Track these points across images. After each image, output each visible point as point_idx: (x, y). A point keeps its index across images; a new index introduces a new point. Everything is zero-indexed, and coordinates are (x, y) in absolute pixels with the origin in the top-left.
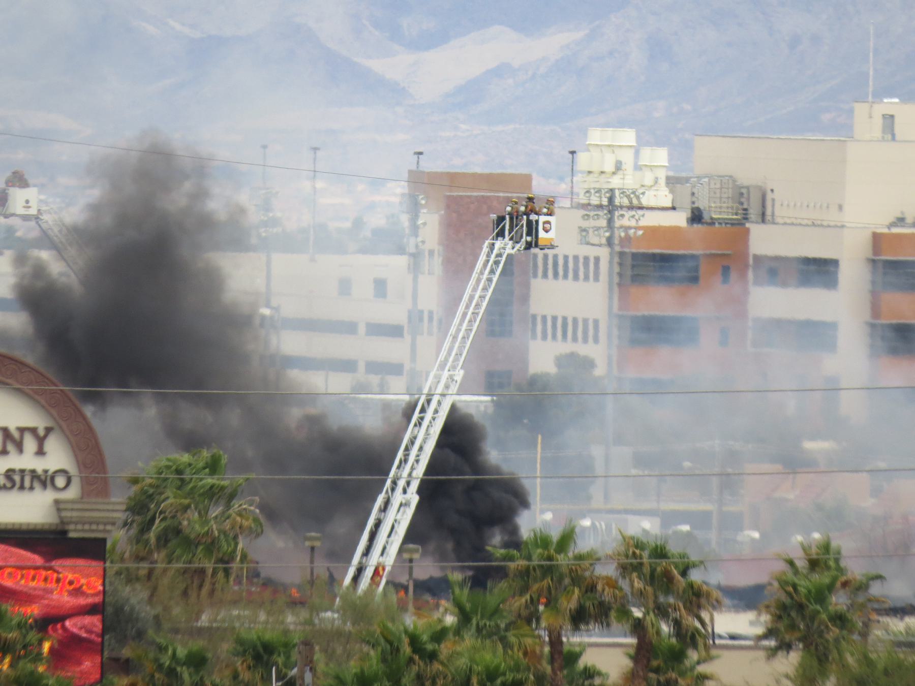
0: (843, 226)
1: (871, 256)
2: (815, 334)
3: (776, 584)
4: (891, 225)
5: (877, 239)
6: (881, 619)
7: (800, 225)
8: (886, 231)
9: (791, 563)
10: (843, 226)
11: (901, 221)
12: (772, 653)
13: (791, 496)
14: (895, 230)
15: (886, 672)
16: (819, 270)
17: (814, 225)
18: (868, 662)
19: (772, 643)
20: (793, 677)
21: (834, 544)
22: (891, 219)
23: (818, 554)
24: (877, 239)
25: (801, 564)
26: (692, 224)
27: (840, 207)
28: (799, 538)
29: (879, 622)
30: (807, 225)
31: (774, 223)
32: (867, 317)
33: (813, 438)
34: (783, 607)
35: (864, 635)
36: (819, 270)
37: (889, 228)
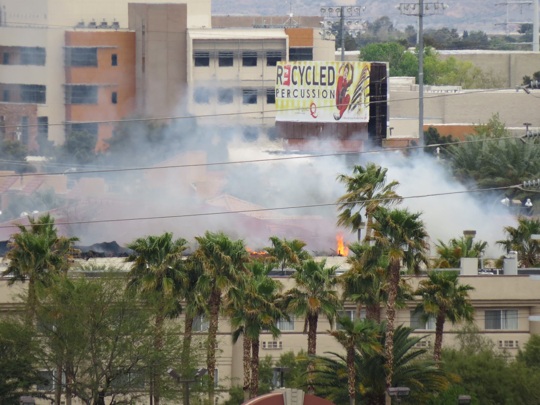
0: (47, 28)
1: (64, 46)
2: (37, 94)
3: (13, 241)
4: (77, 27)
5: (68, 36)
6: (77, 260)
7: (21, 27)
8: (72, 30)
9: (23, 229)
10: (47, 28)
11: (81, 24)
12: (12, 281)
13: (21, 189)
14: (78, 30)
15: (78, 291)
16: (38, 56)
17: (30, 27)
18: (69, 284)
19: (11, 276)
20: (345, 358)
21: (51, 218)
22: (75, 24)
23: (39, 223)
24: (68, 36)
25: (29, 228)
26: (524, 78)
27: (45, 17)
28: (26, 214)
29: (73, 261)
30: (26, 27)
31: (6, 26)
32: (64, 82)
33: (33, 154)
34: (18, 254)
35: (66, 270)
36: (38, 56)
37: (75, 29)
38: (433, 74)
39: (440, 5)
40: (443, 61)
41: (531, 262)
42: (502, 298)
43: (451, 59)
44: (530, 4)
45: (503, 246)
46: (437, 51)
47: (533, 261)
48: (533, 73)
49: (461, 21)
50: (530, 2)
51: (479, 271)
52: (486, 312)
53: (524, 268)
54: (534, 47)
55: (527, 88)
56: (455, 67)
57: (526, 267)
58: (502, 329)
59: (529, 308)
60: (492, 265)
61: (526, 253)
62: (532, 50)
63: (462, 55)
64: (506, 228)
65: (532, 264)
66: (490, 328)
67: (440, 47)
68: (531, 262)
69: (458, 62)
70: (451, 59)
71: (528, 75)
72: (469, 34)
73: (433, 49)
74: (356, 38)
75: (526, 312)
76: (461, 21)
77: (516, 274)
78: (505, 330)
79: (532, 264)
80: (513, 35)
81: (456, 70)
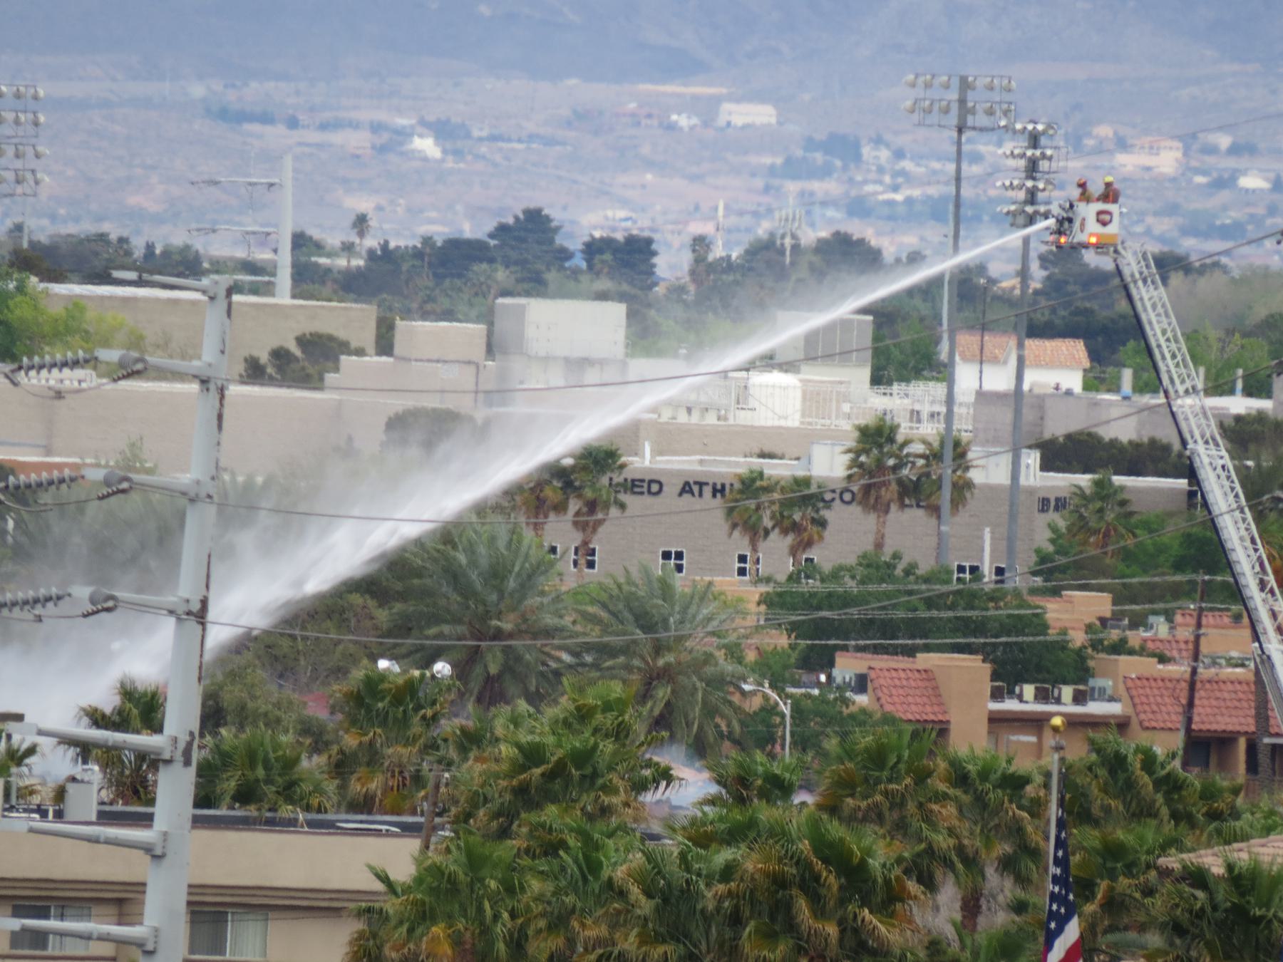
26: (246, 360)
38: (30, 339)
39: (29, 176)
40: (56, 310)
41: (136, 792)
42: (268, 884)
43: (76, 305)
44: (271, 185)
45: (72, 752)
46: (43, 285)
47: (141, 790)
48: (269, 349)
49: (158, 220)
50: (272, 181)
51: (5, 810)
52: (15, 907)
53: (119, 807)
54: (278, 289)
55: (13, 371)
56: (85, 326)
57: (126, 804)
58: (49, 952)
59: (120, 902)
60: (44, 796)
61: (127, 772)
62: (273, 295)
63: (102, 298)
64: (84, 710)
65: (139, 798)
66: (22, 948)
67: (57, 276)
68: (136, 792)
69: (91, 314)
70: (76, 305)
71: (256, 353)
72: (158, 252)
73: (34, 279)
74: (367, 267)
75: (112, 910)
76: (158, 220)
77: (94, 818)
78: (57, 953)
79: (139, 798)
80: (263, 260)
81: (86, 332)
